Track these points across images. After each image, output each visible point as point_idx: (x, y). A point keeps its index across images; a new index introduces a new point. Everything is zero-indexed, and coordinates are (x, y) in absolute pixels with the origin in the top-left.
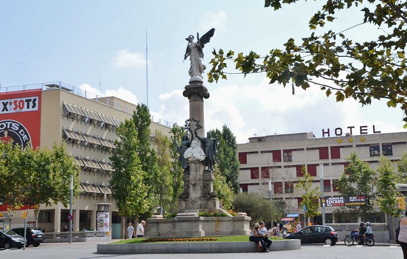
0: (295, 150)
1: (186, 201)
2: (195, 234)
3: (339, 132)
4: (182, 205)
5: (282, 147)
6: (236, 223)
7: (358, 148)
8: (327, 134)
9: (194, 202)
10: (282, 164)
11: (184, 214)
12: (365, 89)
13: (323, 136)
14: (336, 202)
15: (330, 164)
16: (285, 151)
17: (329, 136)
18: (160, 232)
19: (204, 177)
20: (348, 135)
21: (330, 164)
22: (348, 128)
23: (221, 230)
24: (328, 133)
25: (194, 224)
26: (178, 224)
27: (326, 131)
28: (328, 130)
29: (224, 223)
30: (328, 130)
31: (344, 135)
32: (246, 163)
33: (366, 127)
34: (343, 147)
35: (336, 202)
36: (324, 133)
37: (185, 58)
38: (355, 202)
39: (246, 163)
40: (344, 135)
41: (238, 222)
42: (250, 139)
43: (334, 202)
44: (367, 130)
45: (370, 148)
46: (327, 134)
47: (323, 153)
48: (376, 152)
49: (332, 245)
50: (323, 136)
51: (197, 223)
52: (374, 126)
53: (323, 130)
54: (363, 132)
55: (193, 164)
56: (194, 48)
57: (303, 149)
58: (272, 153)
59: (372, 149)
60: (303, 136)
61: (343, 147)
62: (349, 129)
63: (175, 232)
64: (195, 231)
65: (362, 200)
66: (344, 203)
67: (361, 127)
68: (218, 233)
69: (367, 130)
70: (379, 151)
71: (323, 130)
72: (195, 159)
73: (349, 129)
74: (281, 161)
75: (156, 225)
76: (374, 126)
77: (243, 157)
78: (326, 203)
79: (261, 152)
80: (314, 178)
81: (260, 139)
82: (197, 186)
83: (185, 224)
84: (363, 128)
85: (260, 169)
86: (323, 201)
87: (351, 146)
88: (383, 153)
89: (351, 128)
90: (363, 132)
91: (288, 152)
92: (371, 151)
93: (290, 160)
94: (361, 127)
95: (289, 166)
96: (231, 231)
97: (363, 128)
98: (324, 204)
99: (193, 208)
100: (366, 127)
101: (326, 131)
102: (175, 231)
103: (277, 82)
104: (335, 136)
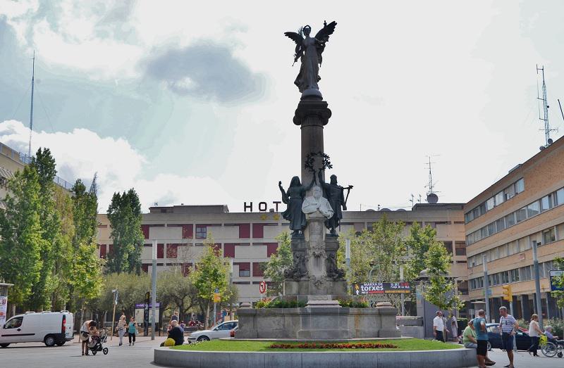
0: (210, 225)
1: (298, 281)
2: (343, 336)
3: (263, 207)
4: (291, 288)
5: (195, 221)
6: (384, 319)
7: (284, 227)
8: (250, 209)
9: (318, 283)
10: (194, 241)
13: (245, 210)
14: (374, 289)
15: (251, 244)
16: (198, 226)
17: (251, 210)
18: (259, 330)
19: (326, 246)
20: (272, 211)
21: (251, 244)
22: (274, 203)
23: (363, 329)
24: (251, 207)
25: (339, 319)
26: (311, 319)
27: (248, 204)
28: (251, 203)
29: (366, 318)
30: (251, 203)
31: (268, 211)
32: (262, 237)
34: (266, 224)
35: (374, 289)
36: (245, 207)
37: (296, 60)
38: (397, 289)
39: (262, 237)
40: (268, 211)
41: (387, 317)
42: (151, 208)
43: (371, 289)
46: (250, 209)
47: (244, 231)
49: (145, 336)
50: (245, 210)
51: (345, 317)
53: (245, 203)
55: (316, 223)
56: (312, 45)
57: (220, 225)
60: (220, 209)
61: (266, 224)
63: (308, 332)
64: (343, 331)
65: (406, 287)
66: (384, 290)
68: (358, 333)
71: (245, 203)
72: (321, 216)
74: (249, 237)
75: (251, 318)
77: (146, 229)
78: (360, 290)
81: (164, 210)
82: (322, 258)
83: (323, 320)
85: (165, 246)
86: (357, 287)
91: (202, 226)
95: (202, 245)
96: (376, 330)
98: (357, 292)
99: (317, 293)
101: (248, 204)
102: (230, 331)
104: (258, 211)
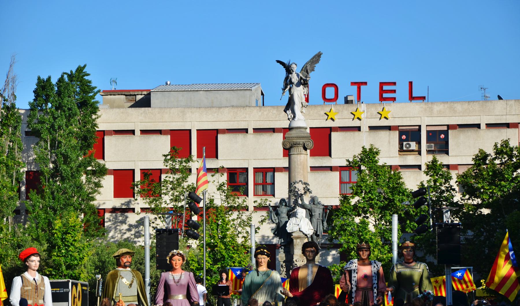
11: (100, 288)
12: (473, 233)
16: (257, 170)
22: (353, 84)
33: (394, 84)
44: (394, 91)
45: (401, 133)
48: (413, 145)
52: (411, 83)
54: (385, 95)
58: (169, 137)
59: (404, 137)
62: (355, 87)
67: (382, 84)
69: (394, 91)
70: (419, 143)
73: (355, 87)
76: (411, 83)
79: (143, 132)
80: (211, 164)
84: (385, 88)
87: (359, 129)
88: (428, 147)
89: (359, 85)
90: (385, 95)
92: (401, 141)
93: (215, 155)
94: (382, 84)
97: (385, 88)
100: (394, 84)
103: (302, 86)
